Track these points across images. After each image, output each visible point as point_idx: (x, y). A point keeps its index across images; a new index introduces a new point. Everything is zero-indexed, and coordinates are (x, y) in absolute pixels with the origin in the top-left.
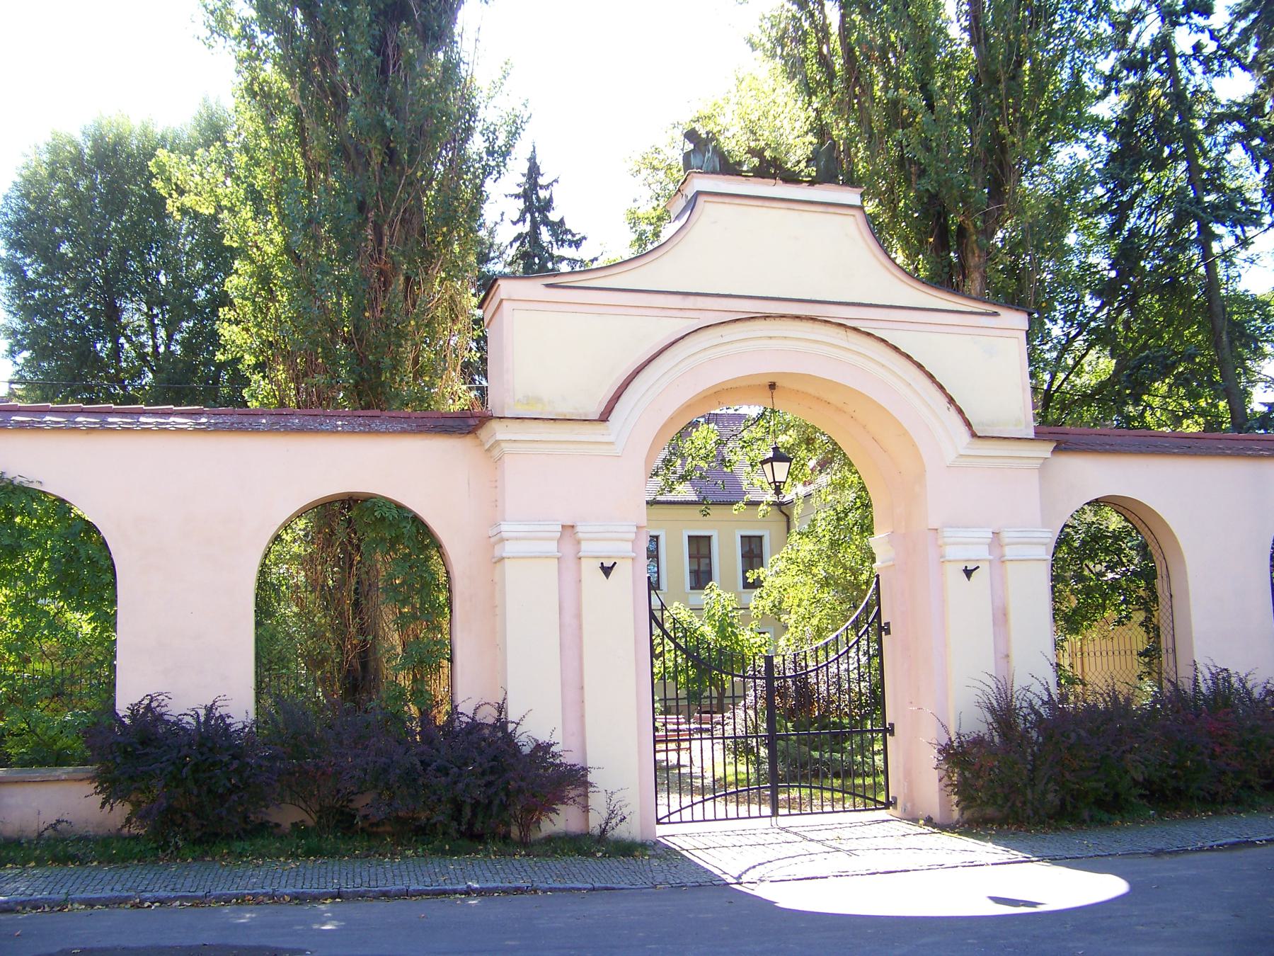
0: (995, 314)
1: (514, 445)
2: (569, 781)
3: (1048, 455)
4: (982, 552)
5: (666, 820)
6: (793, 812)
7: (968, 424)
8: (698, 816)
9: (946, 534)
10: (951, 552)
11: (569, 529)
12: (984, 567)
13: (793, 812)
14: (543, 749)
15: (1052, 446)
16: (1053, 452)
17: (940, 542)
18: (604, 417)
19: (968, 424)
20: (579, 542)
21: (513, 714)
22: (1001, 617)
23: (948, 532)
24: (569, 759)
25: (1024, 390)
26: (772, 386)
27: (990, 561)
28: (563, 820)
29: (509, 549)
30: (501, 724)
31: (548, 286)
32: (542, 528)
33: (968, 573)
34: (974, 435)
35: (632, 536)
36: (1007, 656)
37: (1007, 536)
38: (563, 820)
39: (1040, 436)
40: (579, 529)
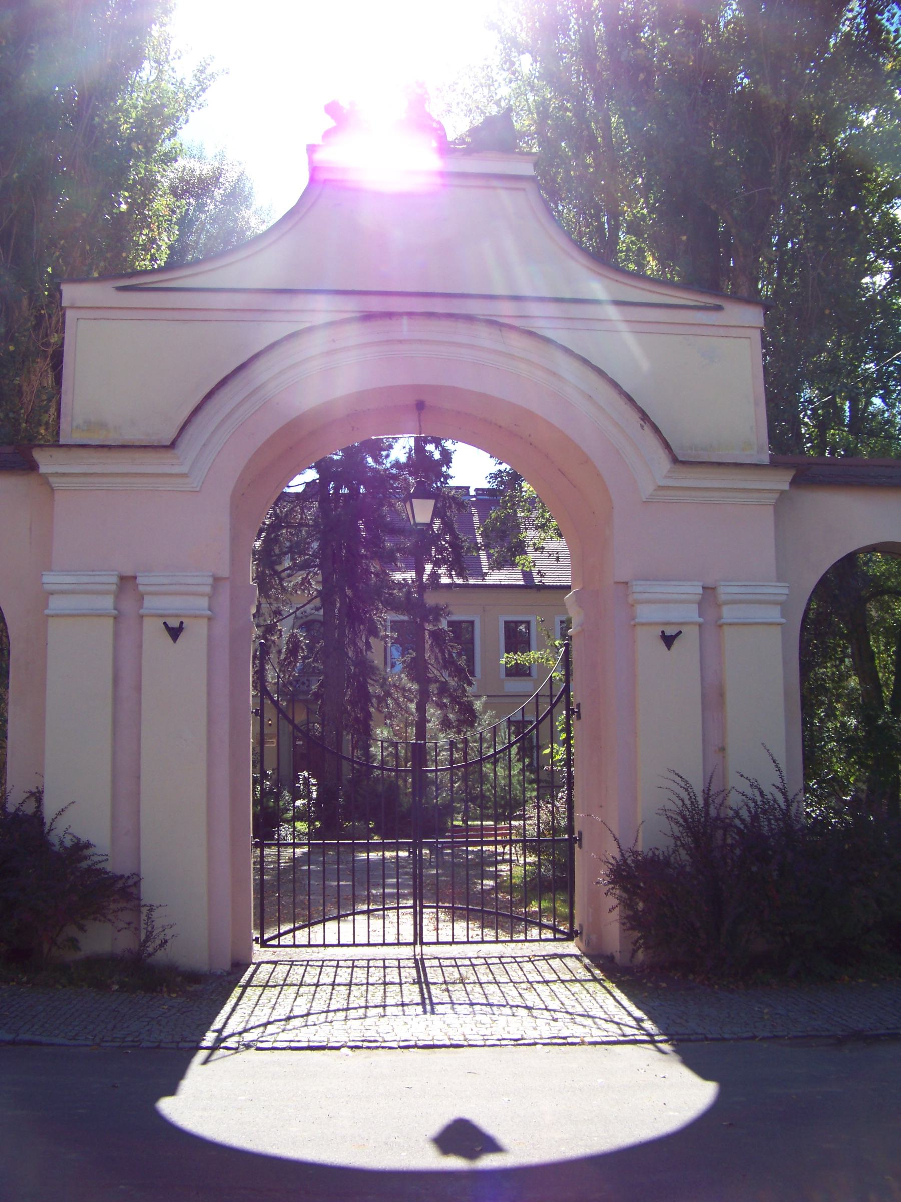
0: (719, 308)
1: (64, 479)
2: (111, 890)
3: (786, 487)
4: (691, 613)
5: (275, 942)
6: (515, 937)
7: (667, 446)
8: (362, 938)
9: (637, 589)
10: (645, 613)
11: (127, 582)
12: (691, 636)
13: (515, 937)
14: (80, 848)
15: (789, 476)
16: (794, 483)
17: (630, 600)
18: (173, 445)
19: (667, 446)
20: (141, 598)
21: (49, 809)
22: (713, 699)
23: (638, 587)
24: (116, 866)
25: (756, 404)
26: (420, 406)
27: (700, 625)
28: (102, 938)
29: (56, 604)
30: (38, 817)
31: (119, 289)
32: (92, 580)
33: (668, 640)
34: (675, 460)
35: (207, 589)
36: (723, 749)
37: (725, 592)
38: (102, 938)
39: (774, 464)
40: (140, 580)
